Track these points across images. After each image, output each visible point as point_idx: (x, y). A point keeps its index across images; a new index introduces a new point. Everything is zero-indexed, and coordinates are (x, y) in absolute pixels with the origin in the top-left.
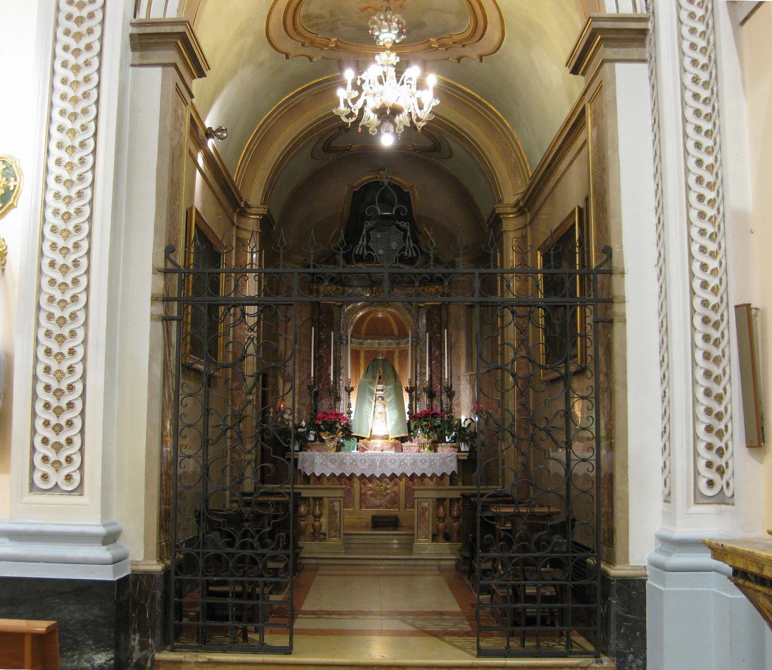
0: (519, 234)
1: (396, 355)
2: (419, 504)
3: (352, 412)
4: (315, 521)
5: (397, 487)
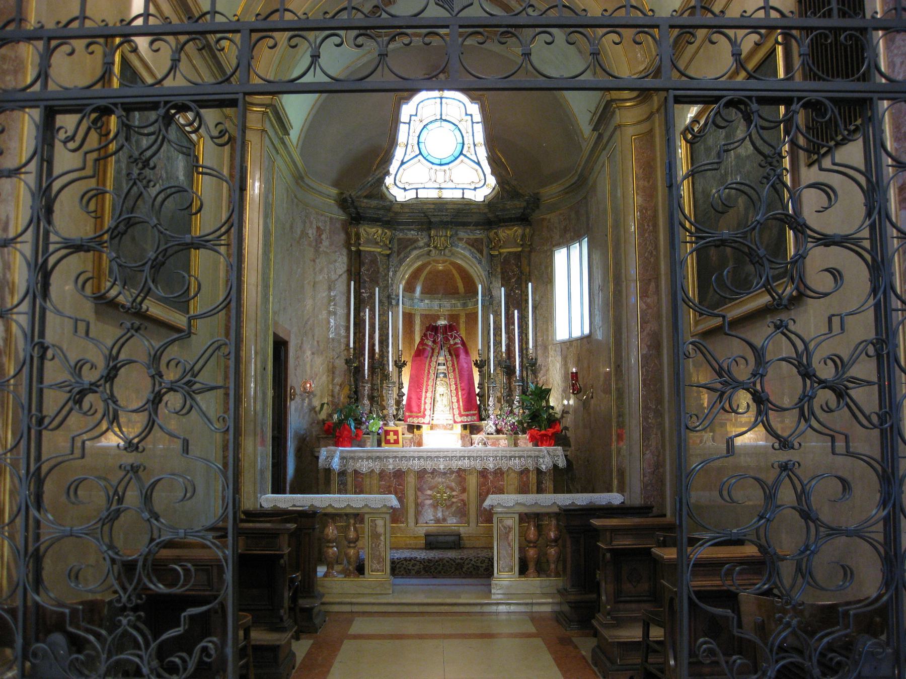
0: (644, 128)
1: (462, 320)
2: (500, 521)
3: (404, 395)
4: (349, 547)
5: (465, 495)
